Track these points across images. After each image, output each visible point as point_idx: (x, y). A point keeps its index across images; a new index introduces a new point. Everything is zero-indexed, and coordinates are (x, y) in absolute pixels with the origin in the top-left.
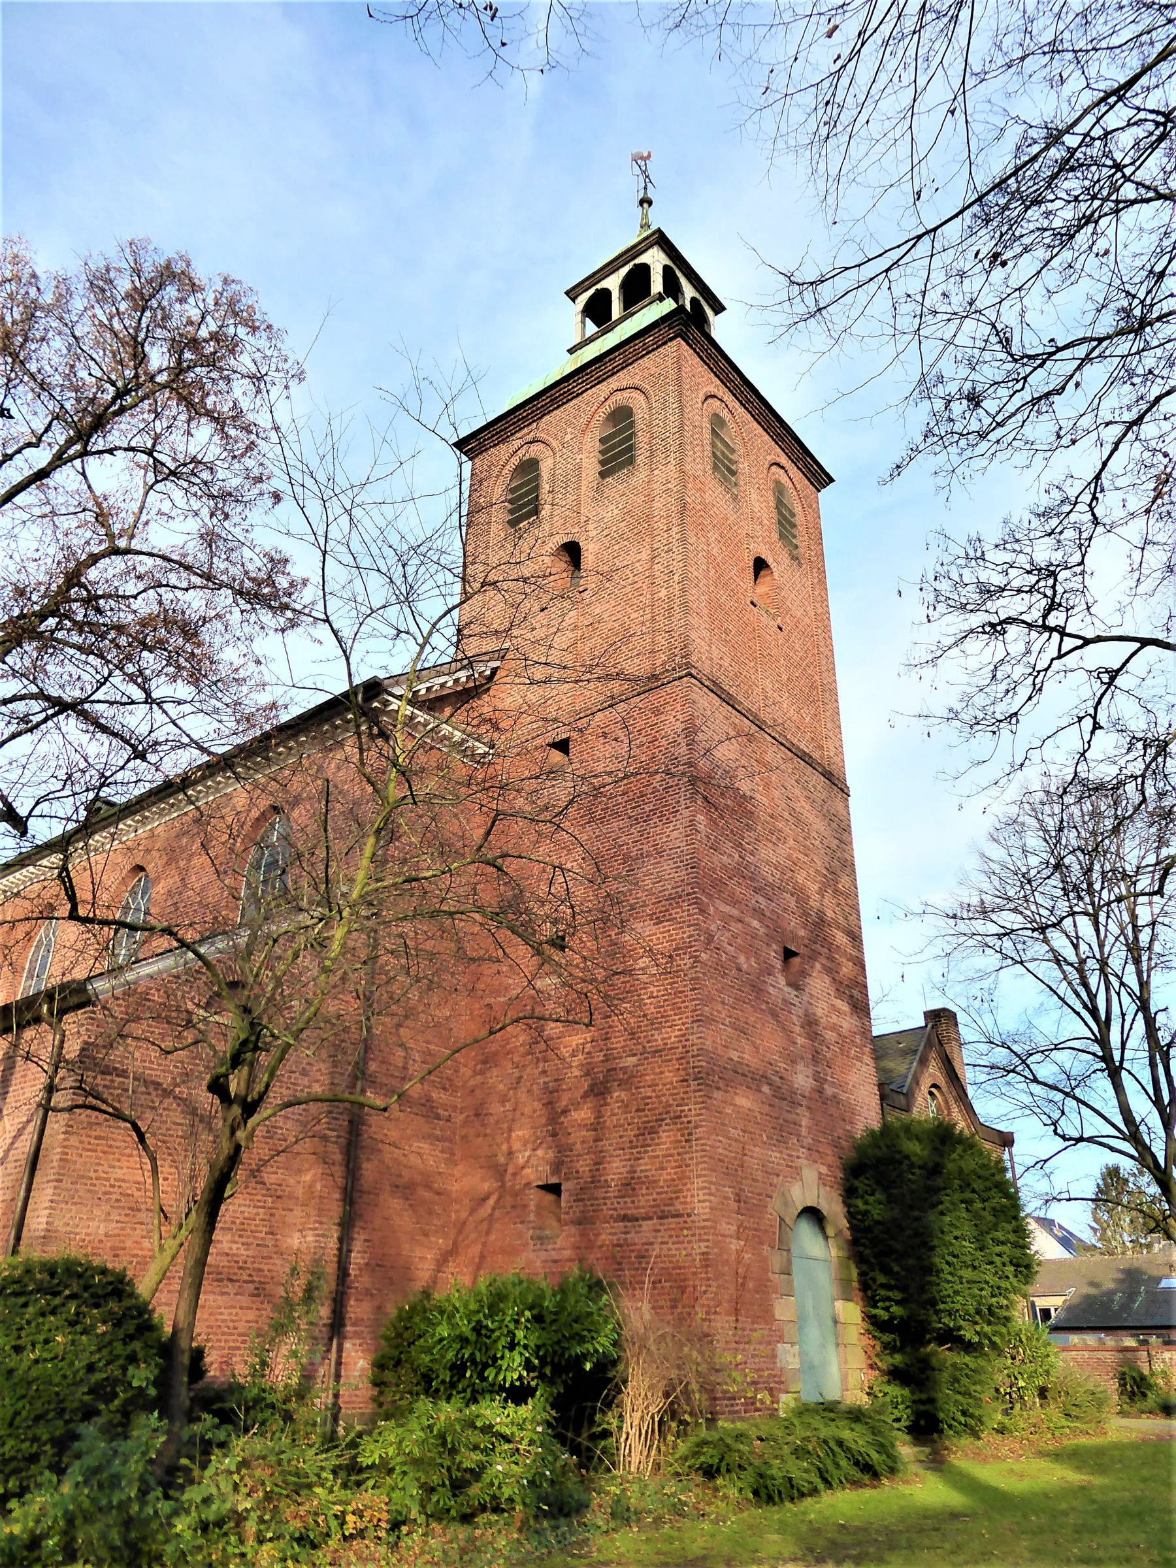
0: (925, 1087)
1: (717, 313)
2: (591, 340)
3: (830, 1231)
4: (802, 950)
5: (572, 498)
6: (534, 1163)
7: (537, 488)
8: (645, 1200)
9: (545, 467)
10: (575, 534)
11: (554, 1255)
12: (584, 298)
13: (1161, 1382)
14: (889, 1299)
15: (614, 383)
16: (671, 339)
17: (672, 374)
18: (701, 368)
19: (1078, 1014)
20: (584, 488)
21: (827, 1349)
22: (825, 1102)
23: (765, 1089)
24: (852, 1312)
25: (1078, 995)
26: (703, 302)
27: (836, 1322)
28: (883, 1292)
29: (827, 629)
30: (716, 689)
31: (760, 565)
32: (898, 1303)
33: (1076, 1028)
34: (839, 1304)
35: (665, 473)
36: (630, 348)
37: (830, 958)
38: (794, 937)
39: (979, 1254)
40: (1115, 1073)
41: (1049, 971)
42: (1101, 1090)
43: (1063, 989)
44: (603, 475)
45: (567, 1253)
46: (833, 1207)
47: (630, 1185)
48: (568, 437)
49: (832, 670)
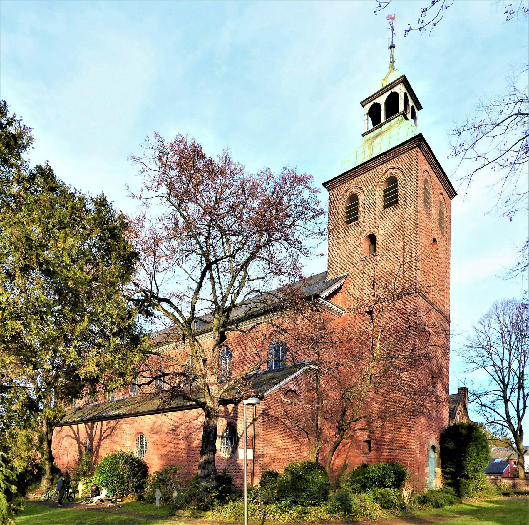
1: (418, 110)
2: (372, 131)
3: (436, 451)
4: (436, 376)
7: (357, 209)
8: (396, 445)
9: (361, 198)
10: (373, 231)
11: (369, 458)
13: (502, 488)
14: (450, 467)
15: (389, 165)
16: (414, 148)
19: (499, 384)
20: (377, 212)
21: (434, 479)
22: (439, 419)
24: (439, 470)
25: (499, 376)
26: (408, 96)
31: (434, 240)
33: (497, 388)
34: (437, 469)
36: (397, 150)
37: (442, 378)
40: (506, 401)
41: (491, 369)
42: (500, 406)
44: (385, 207)
46: (437, 446)
47: (392, 441)
48: (370, 187)
49: (449, 278)
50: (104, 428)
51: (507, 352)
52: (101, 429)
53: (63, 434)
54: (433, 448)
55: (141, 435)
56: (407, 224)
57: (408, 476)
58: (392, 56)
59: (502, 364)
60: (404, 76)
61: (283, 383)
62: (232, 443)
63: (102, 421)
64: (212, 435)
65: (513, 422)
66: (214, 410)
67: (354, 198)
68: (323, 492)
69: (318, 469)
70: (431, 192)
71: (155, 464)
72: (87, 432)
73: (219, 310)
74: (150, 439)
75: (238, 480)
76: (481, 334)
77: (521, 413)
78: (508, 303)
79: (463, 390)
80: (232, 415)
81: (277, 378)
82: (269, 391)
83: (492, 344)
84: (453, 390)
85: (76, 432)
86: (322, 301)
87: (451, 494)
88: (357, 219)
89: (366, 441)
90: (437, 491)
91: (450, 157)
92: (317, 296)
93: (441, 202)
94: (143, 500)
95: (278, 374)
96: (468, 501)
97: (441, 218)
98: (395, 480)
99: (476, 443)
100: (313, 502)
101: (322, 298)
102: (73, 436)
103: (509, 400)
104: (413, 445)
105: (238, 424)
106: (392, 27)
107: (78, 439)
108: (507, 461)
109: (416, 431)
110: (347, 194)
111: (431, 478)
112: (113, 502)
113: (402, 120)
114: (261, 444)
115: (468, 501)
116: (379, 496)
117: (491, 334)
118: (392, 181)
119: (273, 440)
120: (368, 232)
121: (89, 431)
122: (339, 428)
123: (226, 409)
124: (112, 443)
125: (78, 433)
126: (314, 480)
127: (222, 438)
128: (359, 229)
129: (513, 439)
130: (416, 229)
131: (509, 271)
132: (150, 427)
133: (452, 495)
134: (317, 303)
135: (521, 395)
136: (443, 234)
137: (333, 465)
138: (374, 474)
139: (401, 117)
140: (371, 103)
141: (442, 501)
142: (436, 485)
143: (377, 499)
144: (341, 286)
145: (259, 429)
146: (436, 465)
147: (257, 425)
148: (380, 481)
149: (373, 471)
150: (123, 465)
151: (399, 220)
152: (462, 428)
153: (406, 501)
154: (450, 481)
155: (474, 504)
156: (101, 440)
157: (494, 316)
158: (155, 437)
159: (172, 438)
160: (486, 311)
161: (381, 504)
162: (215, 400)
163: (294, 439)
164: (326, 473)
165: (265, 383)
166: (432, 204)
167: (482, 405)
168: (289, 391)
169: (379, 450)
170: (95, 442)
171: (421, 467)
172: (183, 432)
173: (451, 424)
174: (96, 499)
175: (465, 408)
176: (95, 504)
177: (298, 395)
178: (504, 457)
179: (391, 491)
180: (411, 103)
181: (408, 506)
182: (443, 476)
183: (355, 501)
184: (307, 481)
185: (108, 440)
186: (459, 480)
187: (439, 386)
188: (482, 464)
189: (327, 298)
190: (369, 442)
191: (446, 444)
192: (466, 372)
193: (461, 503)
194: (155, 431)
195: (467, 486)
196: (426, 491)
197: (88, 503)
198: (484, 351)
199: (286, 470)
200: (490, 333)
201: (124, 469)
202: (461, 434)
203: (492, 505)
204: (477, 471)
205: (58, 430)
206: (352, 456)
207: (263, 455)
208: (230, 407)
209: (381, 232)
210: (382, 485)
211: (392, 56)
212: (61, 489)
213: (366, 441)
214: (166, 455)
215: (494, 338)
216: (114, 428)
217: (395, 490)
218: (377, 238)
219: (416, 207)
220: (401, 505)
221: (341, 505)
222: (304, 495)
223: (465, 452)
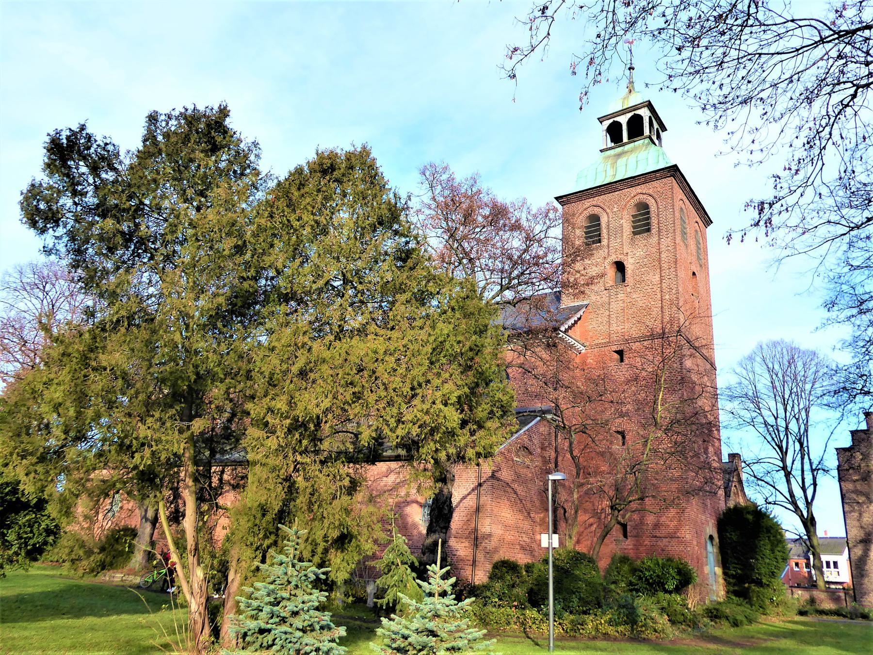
3: (714, 543)
5: (619, 240)
7: (599, 230)
8: (663, 532)
9: (604, 220)
10: (621, 258)
12: (607, 123)
24: (719, 571)
31: (694, 274)
34: (716, 568)
40: (788, 475)
41: (762, 429)
45: (630, 547)
46: (716, 536)
47: (657, 526)
48: (615, 210)
54: (711, 538)
56: (663, 255)
58: (631, 77)
67: (595, 219)
70: (687, 221)
76: (743, 380)
86: (561, 334)
92: (556, 329)
93: (696, 231)
96: (765, 620)
104: (687, 533)
110: (585, 212)
113: (648, 144)
118: (643, 208)
120: (614, 258)
128: (602, 253)
135: (807, 466)
136: (701, 266)
139: (647, 140)
140: (611, 121)
147: (482, 492)
151: (654, 250)
152: (748, 513)
157: (758, 359)
160: (747, 352)
180: (656, 126)
184: (577, 579)
186: (749, 588)
189: (566, 331)
200: (754, 379)
202: (747, 520)
207: (490, 535)
209: (631, 261)
215: (760, 386)
218: (626, 266)
219: (675, 239)
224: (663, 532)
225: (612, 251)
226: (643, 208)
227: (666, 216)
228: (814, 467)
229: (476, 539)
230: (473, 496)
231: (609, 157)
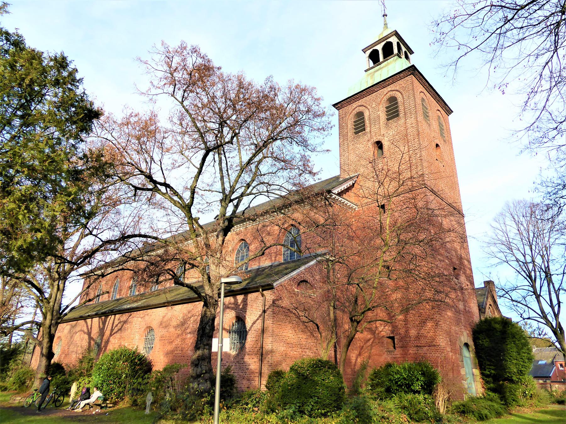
0: (488, 306)
3: (471, 349)
4: (458, 268)
5: (377, 126)
6: (384, 330)
7: (364, 122)
8: (423, 341)
9: (366, 114)
11: (394, 356)
12: (369, 52)
14: (490, 369)
15: (389, 88)
17: (411, 87)
18: (418, 83)
20: (381, 123)
21: (473, 384)
22: (467, 313)
23: (453, 309)
24: (477, 372)
25: (524, 272)
26: (401, 44)
27: (473, 375)
28: (488, 367)
29: (454, 163)
30: (432, 191)
31: (437, 145)
32: (493, 369)
34: (474, 370)
35: (411, 121)
38: (456, 264)
39: (518, 356)
40: (538, 297)
41: (515, 264)
42: (532, 301)
43: (520, 271)
44: (388, 119)
45: (398, 356)
46: (471, 343)
47: (418, 337)
48: (374, 106)
50: (116, 322)
51: (527, 248)
52: (113, 323)
53: (78, 329)
55: (150, 329)
57: (440, 379)
58: (385, 21)
59: (525, 259)
60: (396, 31)
61: (294, 273)
62: (240, 338)
63: (115, 315)
64: (209, 326)
65: (549, 318)
66: (213, 298)
67: (360, 115)
68: (334, 398)
69: (329, 368)
70: (429, 108)
71: (159, 361)
72: (99, 327)
73: (226, 199)
74: (159, 333)
75: (245, 382)
77: (556, 309)
78: (519, 203)
79: (489, 284)
80: (241, 307)
81: (290, 268)
82: (280, 281)
83: (511, 240)
84: (479, 283)
85: (89, 327)
87: (496, 402)
88: (364, 130)
89: (389, 337)
90: (478, 398)
91: (432, 44)
92: (329, 192)
94: (137, 405)
95: (292, 265)
96: (519, 411)
97: (441, 129)
98: (425, 384)
99: (514, 339)
100: (323, 411)
101: (334, 194)
102: (86, 331)
103: (540, 295)
104: (442, 341)
105: (247, 317)
106: (383, 4)
107: (89, 334)
108: (553, 363)
109: (444, 326)
110: (354, 111)
111: (468, 381)
112: (102, 408)
113: (397, 59)
114: (271, 339)
115: (519, 411)
116: (406, 404)
117: (508, 231)
118: (393, 100)
119: (284, 334)
121: (101, 326)
122: (351, 319)
123: (236, 300)
124: (121, 338)
125: (91, 328)
126: (323, 382)
127: (230, 332)
129: (554, 338)
130: (418, 135)
131: (512, 132)
132: (160, 320)
133: (497, 403)
134: (330, 198)
136: (444, 141)
137: (355, 365)
138: (399, 376)
140: (371, 50)
141: (486, 412)
142: (477, 390)
143: (404, 408)
144: (353, 184)
145: (269, 323)
146: (473, 366)
148: (406, 384)
149: (398, 372)
150: (123, 362)
151: (402, 129)
152: (496, 323)
153: (442, 411)
154: (492, 385)
155: (526, 416)
156: (111, 335)
157: (508, 215)
158: (163, 332)
159: (179, 332)
161: (409, 415)
162: (215, 287)
163: (309, 333)
164: (338, 373)
165: (277, 273)
166: (431, 118)
167: (512, 300)
168: (302, 281)
169: (404, 347)
170: (105, 338)
171: (456, 368)
172: (191, 326)
173: (483, 319)
174: (83, 403)
175: (495, 302)
176: (81, 410)
177: (312, 287)
178: (547, 359)
179: (421, 397)
180: (404, 49)
181: (445, 417)
182: (483, 379)
183: (376, 411)
184: (315, 383)
185: (117, 335)
186: (503, 384)
187: (463, 278)
188: (526, 365)
189: (339, 194)
190: (392, 338)
191: (480, 341)
192: (489, 263)
193: (511, 414)
194: (164, 325)
195: (513, 391)
196: (466, 398)
197: (74, 409)
198: (503, 246)
199: (292, 369)
200: (506, 230)
201: (123, 367)
203: (548, 417)
204: (522, 373)
205: (73, 325)
206: (376, 355)
207: (272, 351)
208: (240, 298)
210: (408, 388)
211: (385, 21)
212: (45, 391)
213: (389, 337)
214: (172, 352)
215: (511, 235)
216: (125, 322)
217: (426, 396)
218: (383, 143)
219: (416, 118)
220: (435, 417)
221: (357, 417)
222: (312, 401)
223: (503, 351)
224: (423, 341)
225: (373, 134)
226: (393, 100)
227: (409, 103)
228: (557, 289)
229: (262, 355)
230: (260, 321)
231: (370, 74)
